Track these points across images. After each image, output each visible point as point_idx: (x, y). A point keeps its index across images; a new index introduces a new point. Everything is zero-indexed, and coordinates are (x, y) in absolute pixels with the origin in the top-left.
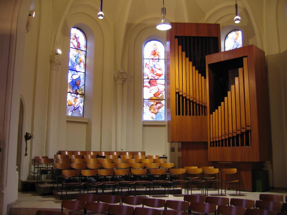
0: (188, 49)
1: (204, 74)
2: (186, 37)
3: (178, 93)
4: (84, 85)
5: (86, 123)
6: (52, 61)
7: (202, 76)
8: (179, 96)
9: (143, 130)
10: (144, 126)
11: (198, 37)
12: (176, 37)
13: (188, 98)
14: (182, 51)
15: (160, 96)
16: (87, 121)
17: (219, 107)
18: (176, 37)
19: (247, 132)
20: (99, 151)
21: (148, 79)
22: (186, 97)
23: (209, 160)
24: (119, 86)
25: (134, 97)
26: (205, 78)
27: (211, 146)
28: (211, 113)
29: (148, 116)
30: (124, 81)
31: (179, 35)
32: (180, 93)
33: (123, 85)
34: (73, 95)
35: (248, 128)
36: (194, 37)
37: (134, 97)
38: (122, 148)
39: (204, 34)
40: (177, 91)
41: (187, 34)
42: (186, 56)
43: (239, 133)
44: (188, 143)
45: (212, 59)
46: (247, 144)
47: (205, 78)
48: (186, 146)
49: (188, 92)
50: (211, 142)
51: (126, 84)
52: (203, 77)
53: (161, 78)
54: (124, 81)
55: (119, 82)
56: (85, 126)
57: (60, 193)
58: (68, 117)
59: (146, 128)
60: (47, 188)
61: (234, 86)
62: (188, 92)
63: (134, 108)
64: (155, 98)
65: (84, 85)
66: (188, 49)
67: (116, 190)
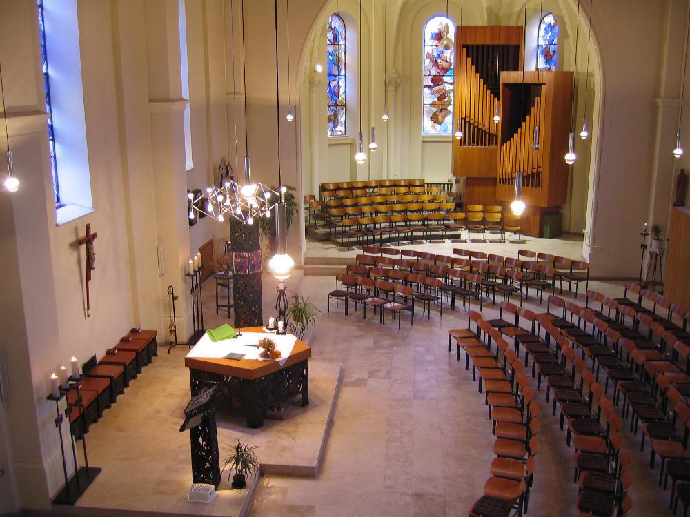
0: (480, 63)
1: (497, 95)
2: (478, 46)
3: (465, 119)
4: (345, 92)
5: (350, 143)
6: (311, 83)
7: (495, 97)
8: (465, 122)
9: (422, 147)
10: (424, 142)
11: (494, 46)
12: (464, 46)
13: (476, 124)
14: (472, 64)
15: (446, 100)
16: (350, 142)
17: (512, 139)
18: (464, 46)
19: (538, 173)
20: (367, 180)
21: (430, 75)
22: (473, 124)
23: (497, 199)
24: (391, 94)
25: (411, 99)
26: (498, 99)
27: (500, 183)
28: (502, 144)
29: (428, 127)
30: (397, 86)
31: (468, 43)
32: (467, 120)
33: (395, 92)
34: (331, 108)
35: (540, 169)
36: (488, 46)
37: (411, 99)
38: (396, 173)
39: (501, 41)
40: (463, 116)
41: (479, 42)
42: (477, 72)
43: (530, 172)
44: (474, 179)
45: (507, 77)
46: (538, 186)
47: (498, 99)
48: (470, 182)
49: (476, 120)
50: (500, 179)
51: (400, 89)
52: (496, 99)
53: (448, 74)
54: (397, 86)
55: (391, 88)
56: (348, 147)
57: (340, 240)
58: (330, 140)
59: (427, 144)
60: (324, 234)
61: (539, 98)
62: (476, 120)
63: (410, 131)
64: (438, 103)
65: (345, 92)
66: (480, 63)
67: (393, 235)
